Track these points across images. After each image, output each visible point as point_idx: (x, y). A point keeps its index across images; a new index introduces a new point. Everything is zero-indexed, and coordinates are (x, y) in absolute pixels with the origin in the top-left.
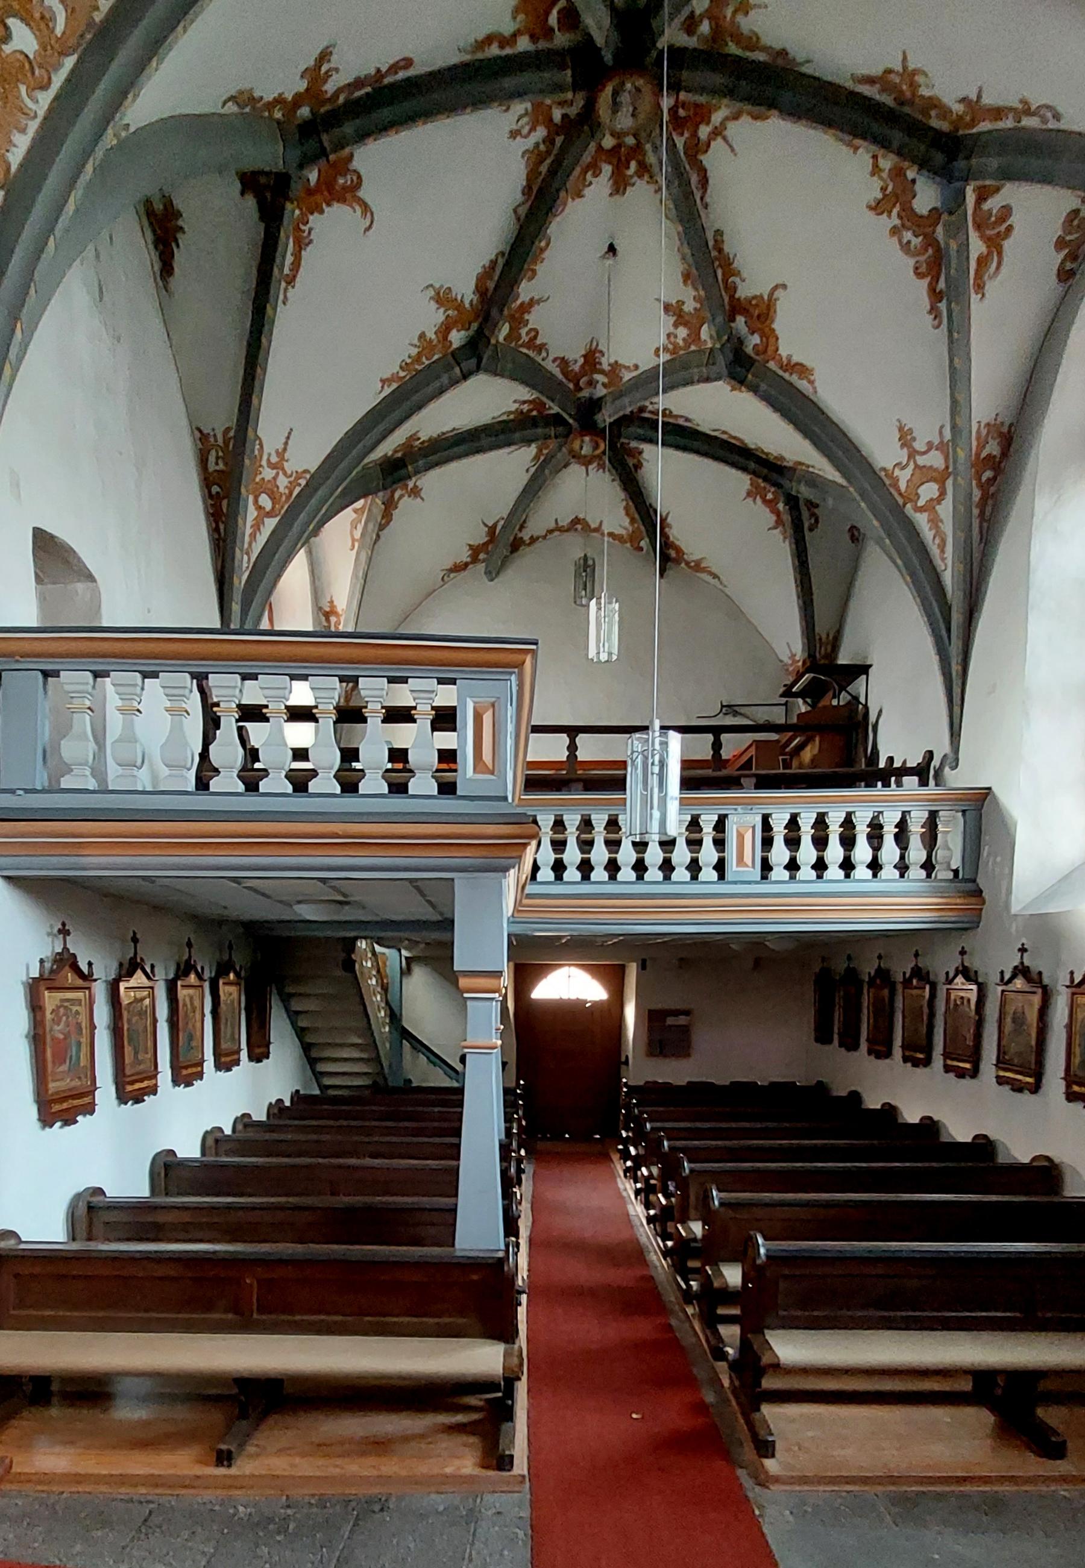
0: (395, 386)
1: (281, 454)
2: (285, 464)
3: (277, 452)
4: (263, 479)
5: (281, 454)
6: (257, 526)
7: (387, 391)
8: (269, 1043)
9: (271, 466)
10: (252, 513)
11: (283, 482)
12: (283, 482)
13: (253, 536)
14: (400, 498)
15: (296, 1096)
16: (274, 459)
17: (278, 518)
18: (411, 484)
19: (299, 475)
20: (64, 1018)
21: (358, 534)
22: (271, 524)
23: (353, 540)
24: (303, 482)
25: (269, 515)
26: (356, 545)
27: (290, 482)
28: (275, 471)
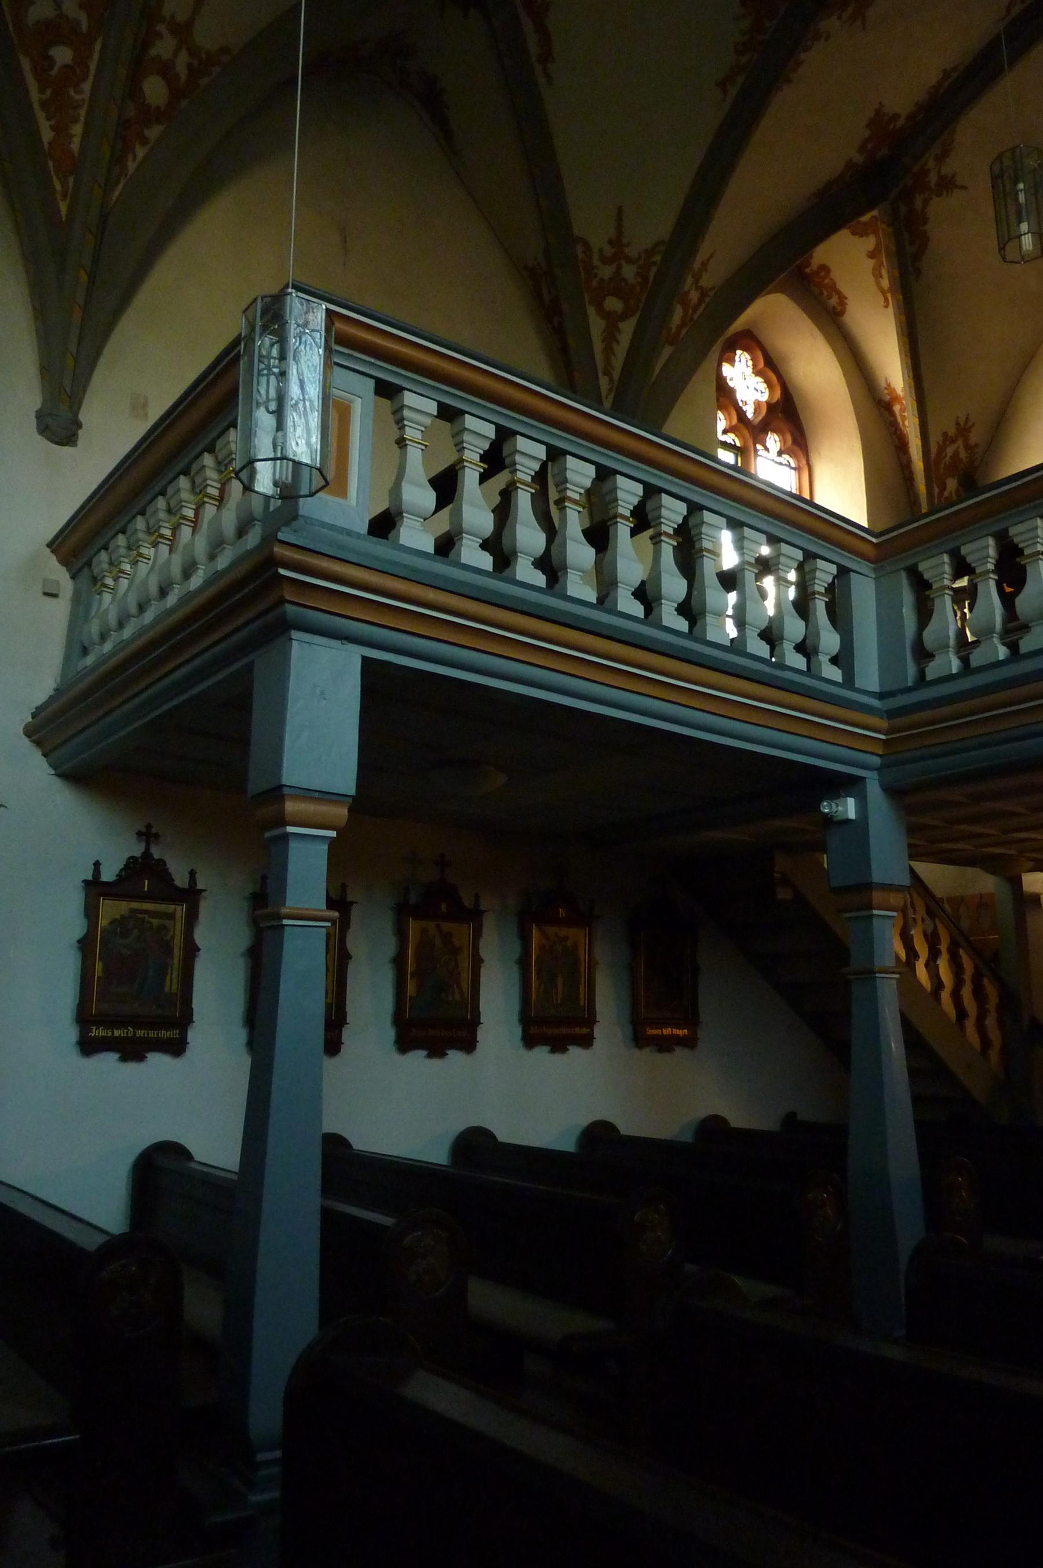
0: (740, 79)
1: (617, 242)
2: (627, 250)
3: (611, 242)
4: (602, 280)
5: (617, 242)
6: (611, 337)
7: (733, 91)
8: (595, 1022)
9: (605, 261)
10: (597, 326)
11: (629, 272)
12: (629, 272)
13: (608, 351)
14: (926, 203)
15: (790, 1120)
16: (609, 251)
17: (638, 315)
18: (933, 178)
19: (650, 253)
20: (136, 932)
21: (885, 283)
22: (627, 329)
23: (883, 292)
24: (658, 258)
25: (625, 316)
26: (889, 296)
27: (596, 275)
28: (615, 265)
